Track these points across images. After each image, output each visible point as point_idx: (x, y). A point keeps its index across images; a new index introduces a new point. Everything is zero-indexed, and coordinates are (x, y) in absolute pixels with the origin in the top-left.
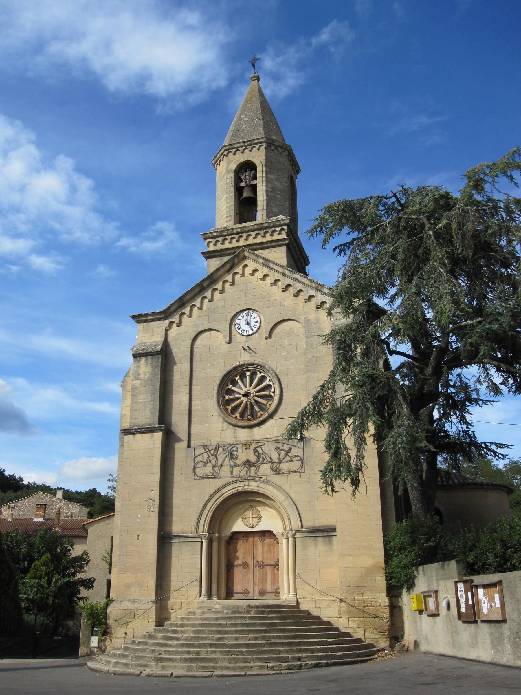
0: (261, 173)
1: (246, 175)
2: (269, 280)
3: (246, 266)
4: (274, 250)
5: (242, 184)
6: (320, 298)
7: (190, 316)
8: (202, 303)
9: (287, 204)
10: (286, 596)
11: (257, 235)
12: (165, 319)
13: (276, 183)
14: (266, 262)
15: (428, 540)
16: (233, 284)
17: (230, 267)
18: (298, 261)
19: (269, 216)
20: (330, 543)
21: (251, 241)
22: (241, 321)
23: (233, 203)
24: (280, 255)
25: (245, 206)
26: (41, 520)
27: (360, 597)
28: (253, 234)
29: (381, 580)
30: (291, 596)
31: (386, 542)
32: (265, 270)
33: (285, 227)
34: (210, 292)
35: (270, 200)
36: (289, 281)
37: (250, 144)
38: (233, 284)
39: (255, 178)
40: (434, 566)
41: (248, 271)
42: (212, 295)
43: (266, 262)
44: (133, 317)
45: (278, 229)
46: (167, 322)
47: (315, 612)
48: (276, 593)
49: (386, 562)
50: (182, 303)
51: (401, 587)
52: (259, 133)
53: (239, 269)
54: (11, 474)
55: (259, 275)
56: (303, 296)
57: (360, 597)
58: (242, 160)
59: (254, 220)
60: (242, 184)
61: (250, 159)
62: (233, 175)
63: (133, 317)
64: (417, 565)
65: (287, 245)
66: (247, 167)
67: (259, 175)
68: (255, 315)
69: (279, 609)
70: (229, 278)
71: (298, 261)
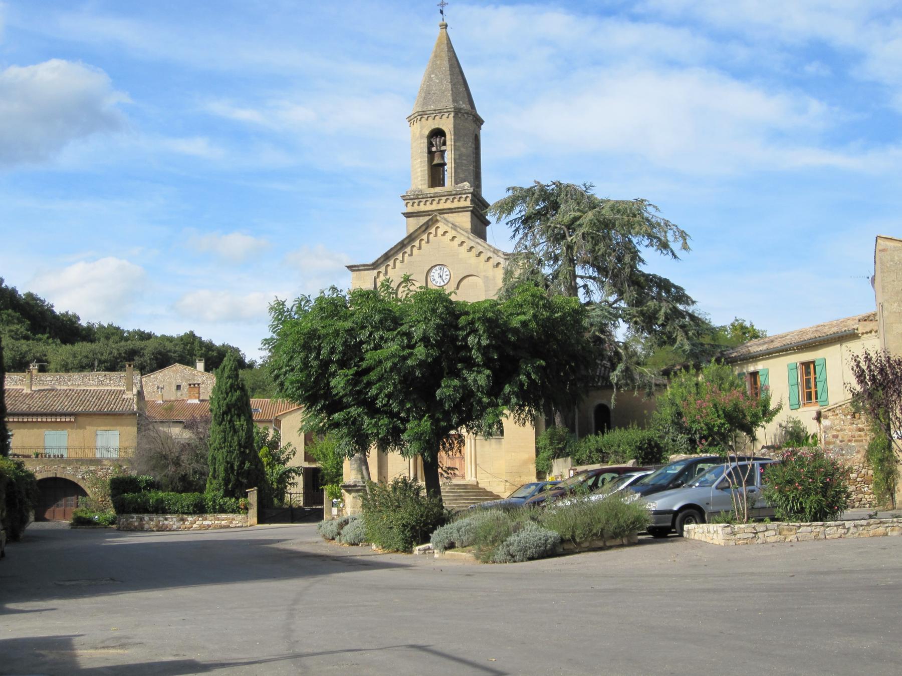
0: (450, 138)
1: (436, 141)
2: (457, 241)
3: (438, 228)
4: (461, 214)
5: (434, 149)
6: (496, 259)
7: (394, 267)
8: (403, 257)
9: (471, 168)
10: (470, 479)
11: (447, 200)
12: (374, 269)
13: (462, 149)
14: (454, 227)
15: (559, 443)
16: (428, 242)
17: (426, 227)
18: (480, 226)
19: (456, 183)
20: (500, 443)
21: (441, 206)
22: (435, 273)
23: (426, 168)
24: (465, 220)
25: (436, 175)
26: (196, 401)
27: (518, 479)
28: (444, 198)
29: (533, 469)
30: (473, 479)
31: (537, 443)
32: (454, 233)
33: (470, 195)
34: (409, 248)
35: (458, 166)
36: (472, 244)
37: (440, 112)
38: (428, 242)
39: (444, 144)
40: (561, 460)
41: (440, 232)
42: (412, 251)
43: (454, 227)
44: (348, 267)
45: (464, 196)
46: (375, 272)
47: (489, 489)
48: (463, 477)
49: (537, 455)
50: (387, 257)
51: (545, 473)
52: (447, 102)
53: (433, 230)
54: (63, 311)
55: (449, 236)
56: (483, 257)
57: (518, 479)
58: (433, 127)
59: (443, 185)
60: (434, 149)
61: (440, 127)
62: (426, 141)
63: (348, 267)
64: (554, 458)
65: (472, 212)
66: (438, 133)
67: (448, 143)
68: (446, 269)
69: (464, 487)
70: (425, 237)
71: (480, 226)
